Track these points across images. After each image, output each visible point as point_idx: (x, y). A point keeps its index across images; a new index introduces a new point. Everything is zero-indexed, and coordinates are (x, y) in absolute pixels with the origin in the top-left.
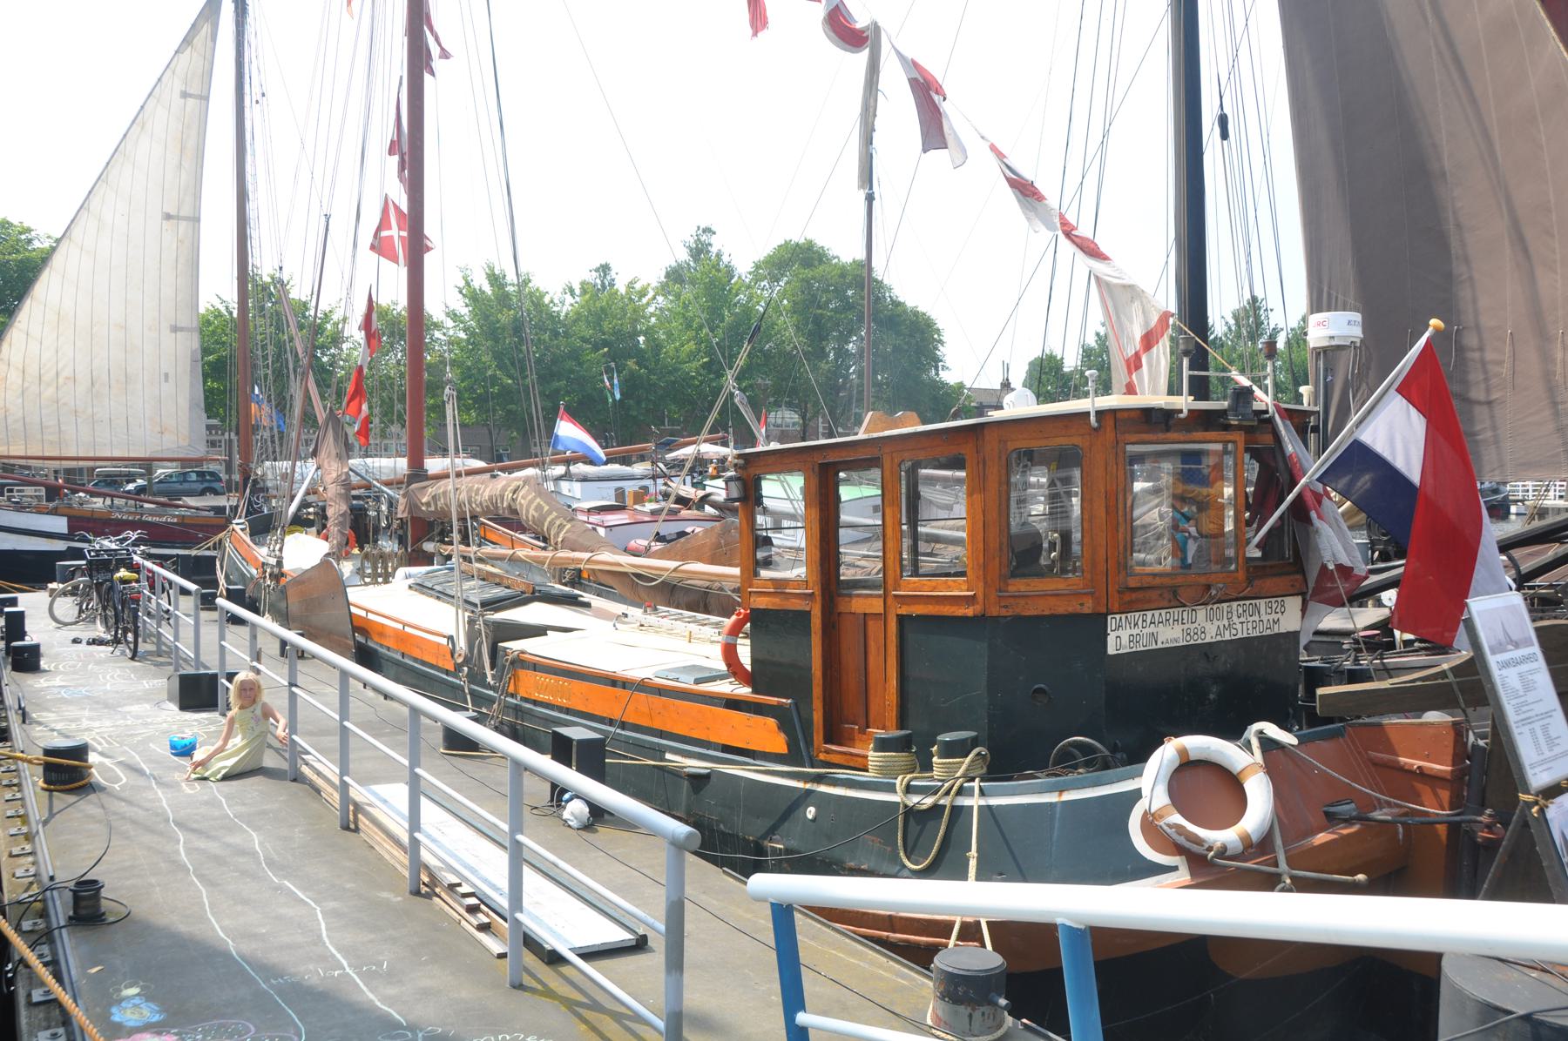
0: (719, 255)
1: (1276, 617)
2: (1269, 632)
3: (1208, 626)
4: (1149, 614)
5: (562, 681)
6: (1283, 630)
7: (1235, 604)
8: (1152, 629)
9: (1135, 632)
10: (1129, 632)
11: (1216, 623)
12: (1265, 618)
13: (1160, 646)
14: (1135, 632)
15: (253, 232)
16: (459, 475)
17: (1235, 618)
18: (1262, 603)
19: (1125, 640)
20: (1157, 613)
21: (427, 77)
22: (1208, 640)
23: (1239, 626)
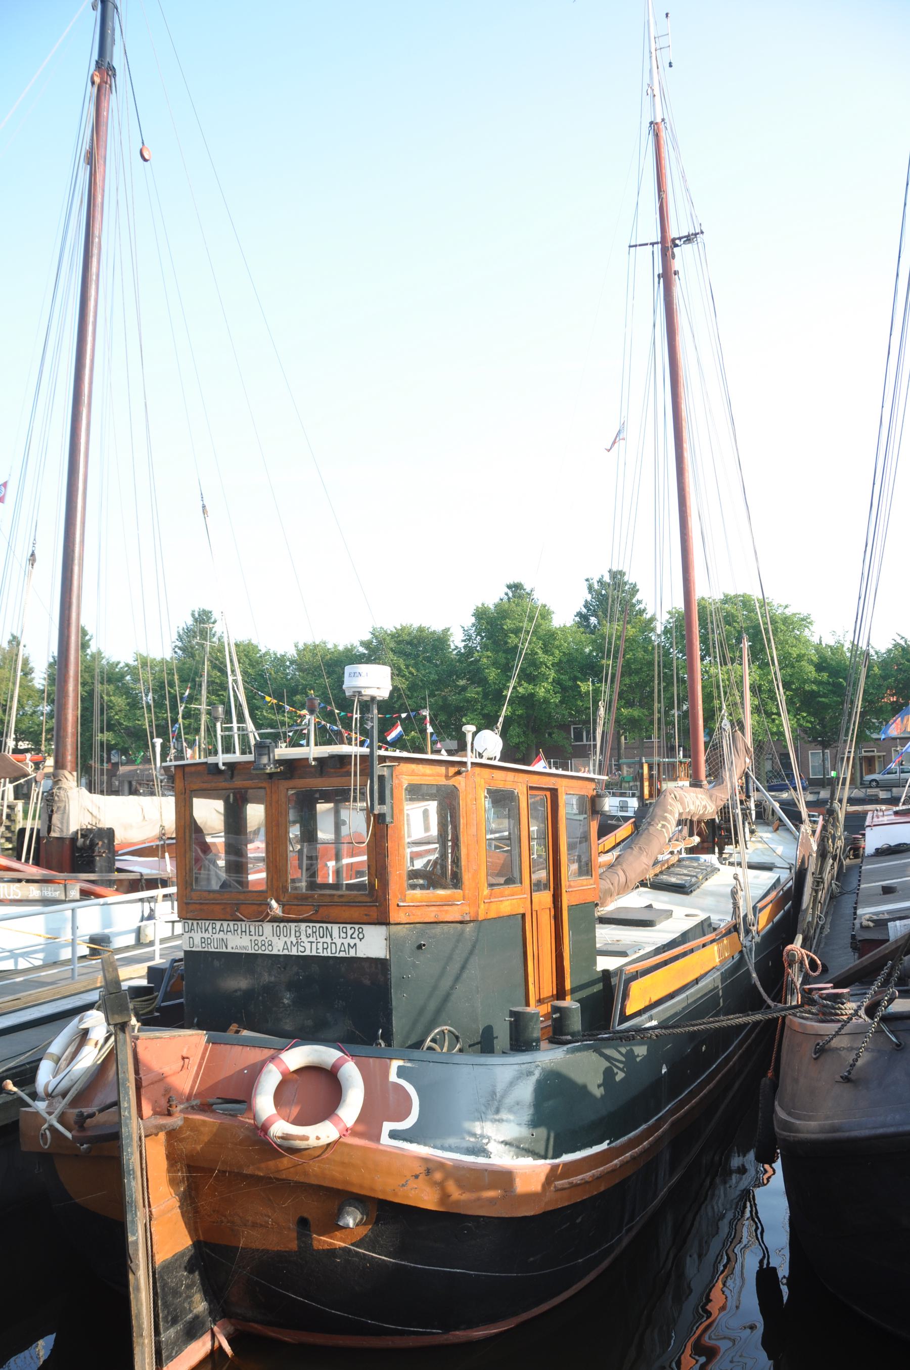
0: (275, 654)
1: (352, 942)
2: (342, 954)
3: (275, 940)
4: (218, 924)
5: (89, 988)
6: (360, 954)
7: (303, 926)
8: (221, 935)
9: (206, 935)
10: (200, 935)
11: (284, 939)
12: (339, 942)
13: (230, 950)
14: (206, 935)
15: (666, 163)
16: (739, 864)
17: (303, 937)
18: (335, 928)
19: (197, 941)
20: (225, 924)
21: (56, 654)
22: (275, 952)
23: (308, 946)
